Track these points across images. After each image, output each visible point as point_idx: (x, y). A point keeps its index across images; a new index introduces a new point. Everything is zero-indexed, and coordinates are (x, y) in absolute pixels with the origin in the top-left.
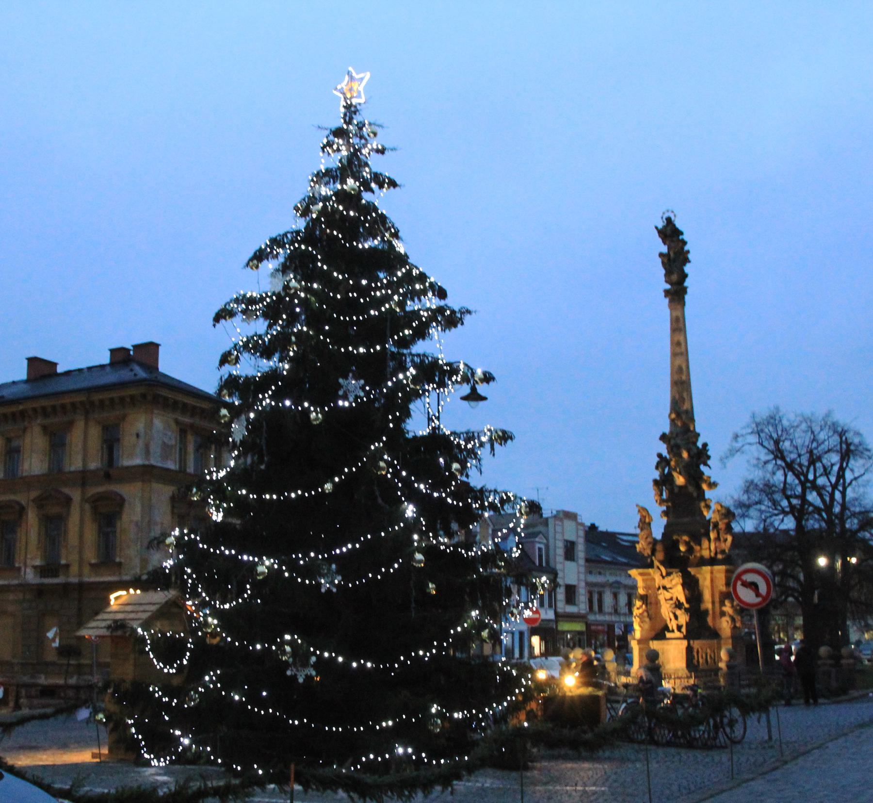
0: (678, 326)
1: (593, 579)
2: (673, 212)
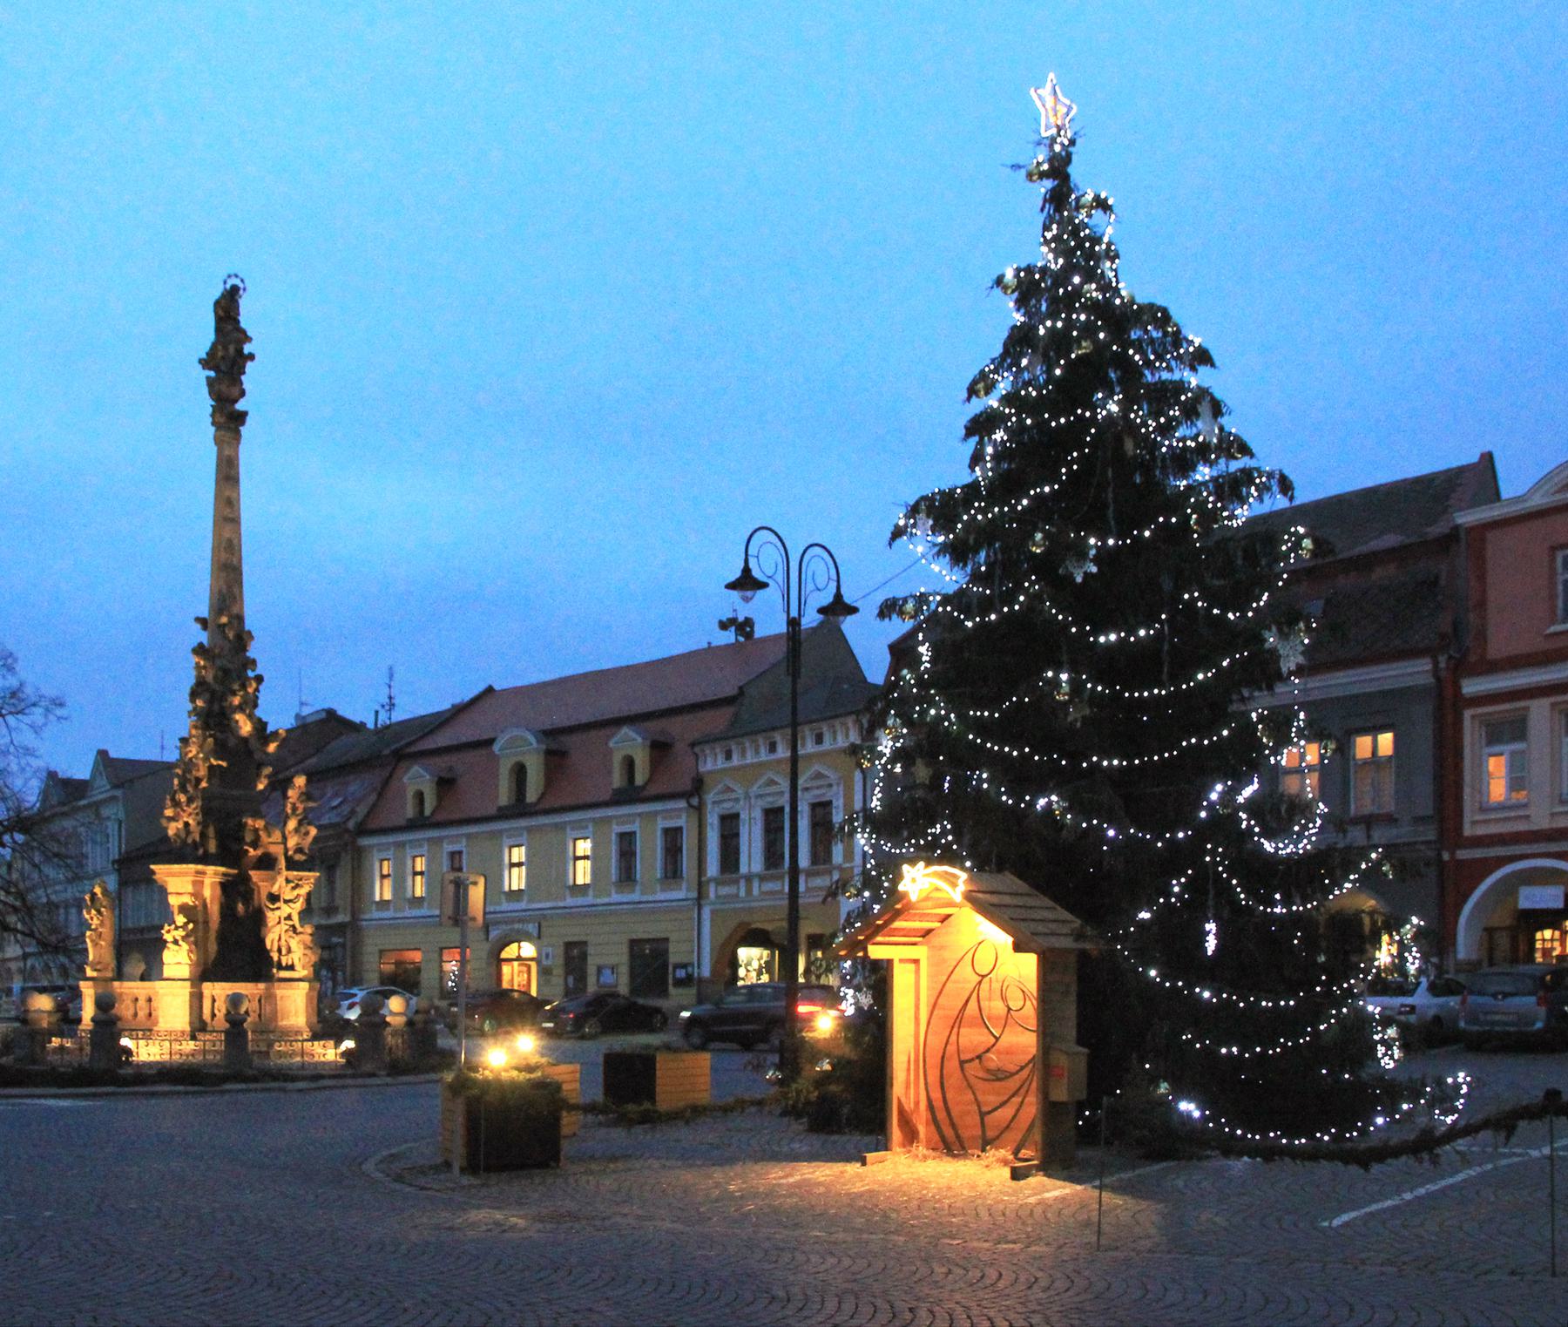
0: (228, 473)
2: (236, 276)
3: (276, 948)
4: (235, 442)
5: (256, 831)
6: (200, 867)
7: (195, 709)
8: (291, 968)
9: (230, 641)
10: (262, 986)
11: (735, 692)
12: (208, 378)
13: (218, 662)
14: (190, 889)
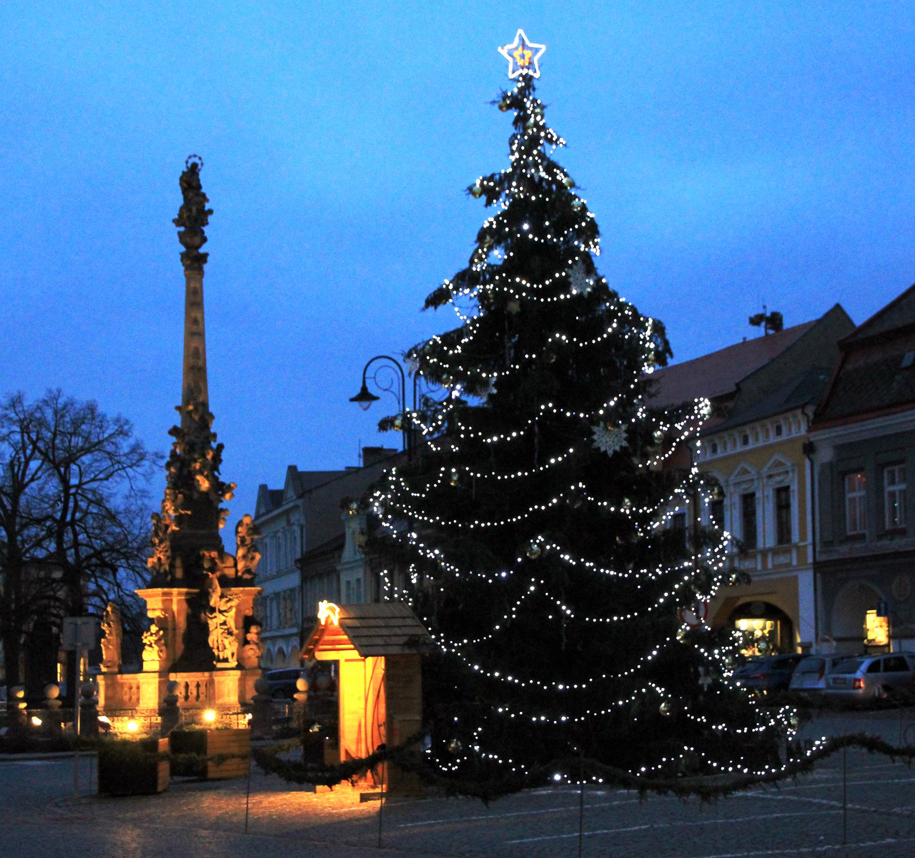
0: (194, 300)
1: (897, 493)
3: (215, 647)
4: (198, 277)
5: (212, 560)
6: (166, 590)
7: (170, 474)
8: (226, 660)
9: (196, 422)
10: (207, 674)
11: (734, 388)
12: (179, 233)
13: (187, 439)
14: (160, 605)
